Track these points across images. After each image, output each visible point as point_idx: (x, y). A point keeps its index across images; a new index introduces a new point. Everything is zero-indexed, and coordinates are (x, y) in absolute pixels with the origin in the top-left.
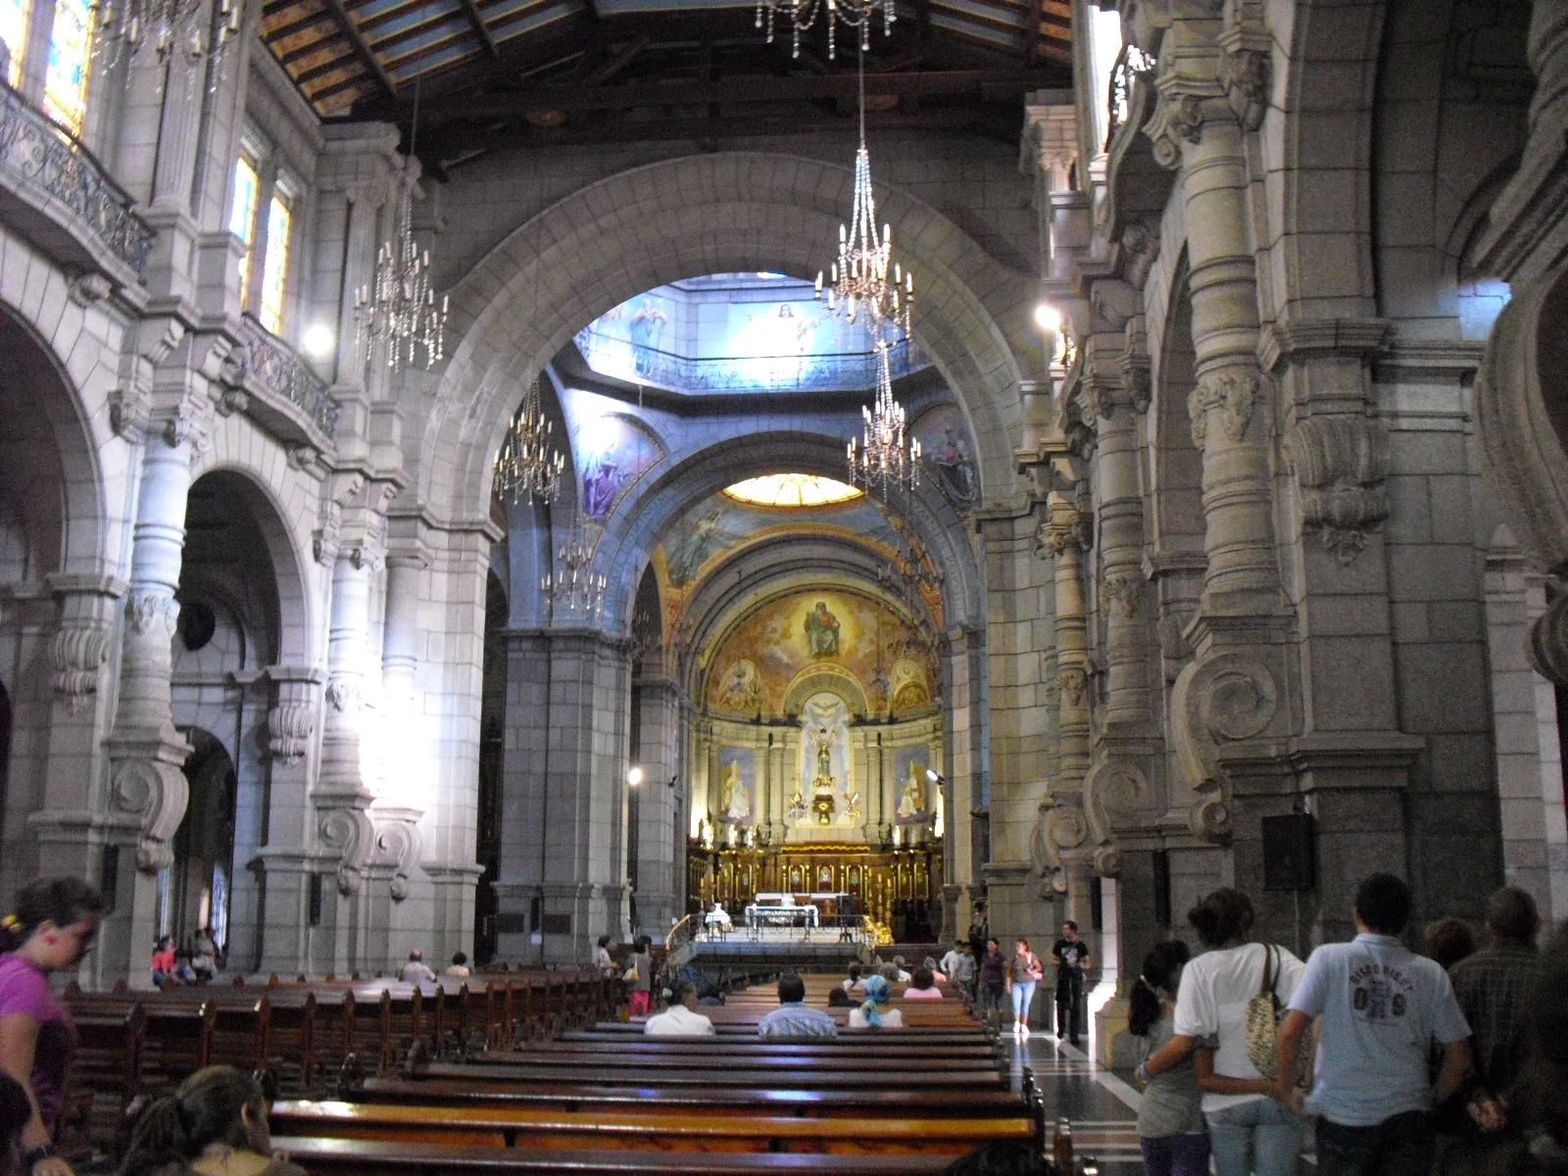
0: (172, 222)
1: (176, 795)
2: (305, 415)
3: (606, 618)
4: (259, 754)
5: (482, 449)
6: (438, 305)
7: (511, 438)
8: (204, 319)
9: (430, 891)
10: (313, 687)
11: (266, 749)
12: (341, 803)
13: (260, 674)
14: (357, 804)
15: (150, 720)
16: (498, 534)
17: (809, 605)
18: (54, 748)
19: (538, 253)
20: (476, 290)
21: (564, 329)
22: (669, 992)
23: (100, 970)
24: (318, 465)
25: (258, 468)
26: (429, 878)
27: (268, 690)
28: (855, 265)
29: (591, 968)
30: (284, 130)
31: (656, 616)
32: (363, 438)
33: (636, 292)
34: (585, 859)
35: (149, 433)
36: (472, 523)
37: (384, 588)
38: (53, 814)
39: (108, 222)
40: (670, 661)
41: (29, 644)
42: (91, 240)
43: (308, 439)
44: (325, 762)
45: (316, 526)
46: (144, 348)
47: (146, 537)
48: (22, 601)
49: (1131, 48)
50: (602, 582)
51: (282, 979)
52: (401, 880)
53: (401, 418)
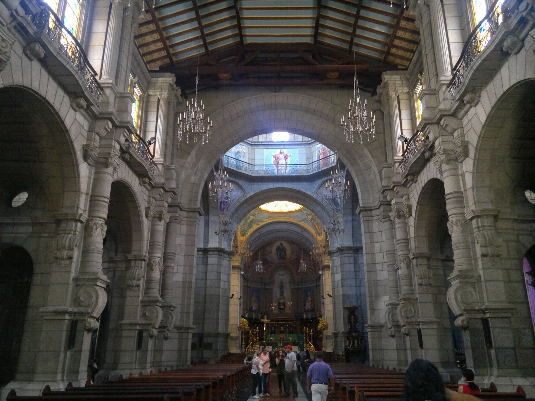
9: (177, 335)
15: (95, 270)
23: (66, 373)
24: (149, 184)
25: (130, 183)
26: (177, 331)
32: (163, 177)
46: (97, 130)
47: (95, 200)
49: (486, 21)
52: (168, 332)
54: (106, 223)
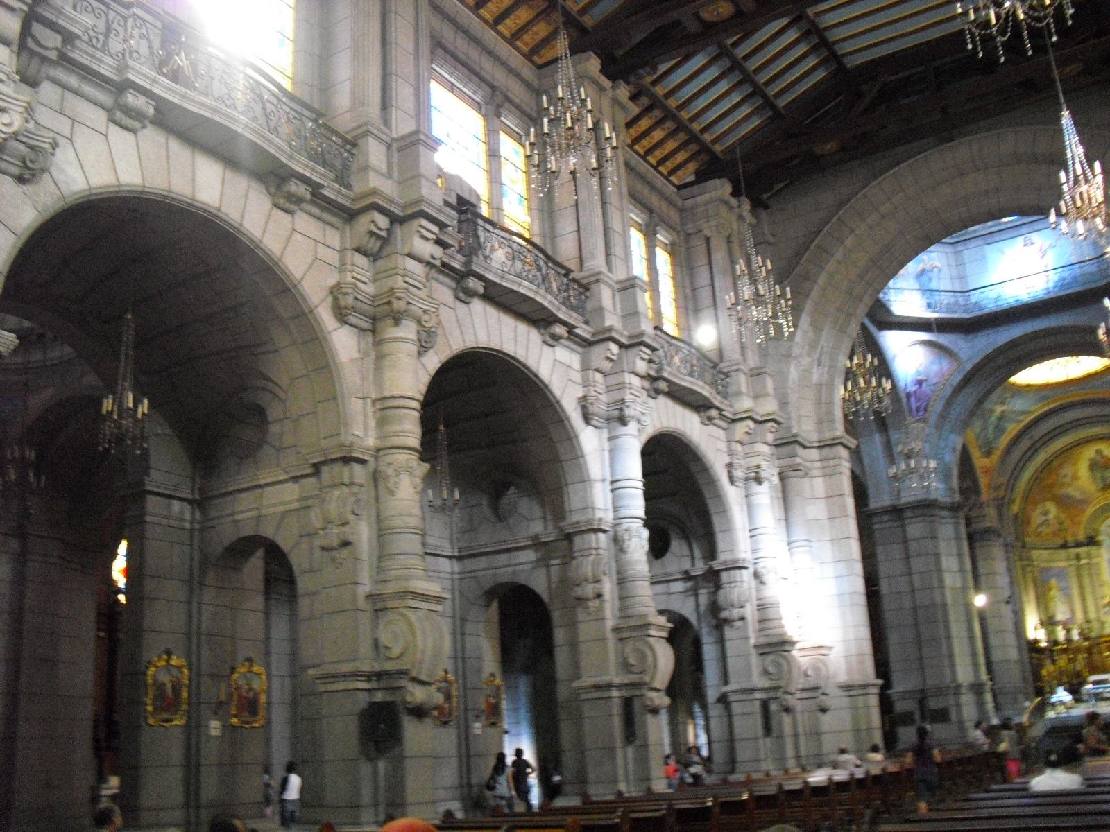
0: (597, 279)
1: (664, 659)
2: (707, 387)
3: (937, 488)
4: (714, 622)
5: (830, 386)
6: (783, 295)
7: (849, 375)
8: (630, 337)
9: (846, 702)
10: (744, 571)
11: (718, 617)
12: (776, 649)
13: (706, 567)
14: (787, 648)
15: (642, 610)
16: (852, 443)
17: (1089, 452)
18: (582, 637)
19: (842, 243)
20: (807, 277)
21: (870, 291)
22: (1035, 760)
24: (721, 419)
26: (846, 693)
27: (713, 578)
28: (1078, 197)
29: (970, 745)
30: (655, 201)
31: (975, 481)
32: (749, 396)
33: (917, 254)
34: (953, 666)
35: (609, 419)
36: (833, 439)
37: (780, 495)
38: (587, 681)
39: (559, 289)
40: (991, 512)
41: (555, 571)
42: (550, 302)
43: (711, 403)
44: (761, 621)
45: (727, 461)
48: (546, 543)
50: (933, 464)
51: (755, 776)
53: (771, 376)
54: (645, 525)
